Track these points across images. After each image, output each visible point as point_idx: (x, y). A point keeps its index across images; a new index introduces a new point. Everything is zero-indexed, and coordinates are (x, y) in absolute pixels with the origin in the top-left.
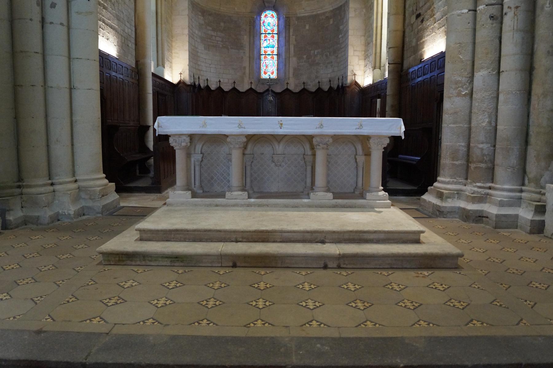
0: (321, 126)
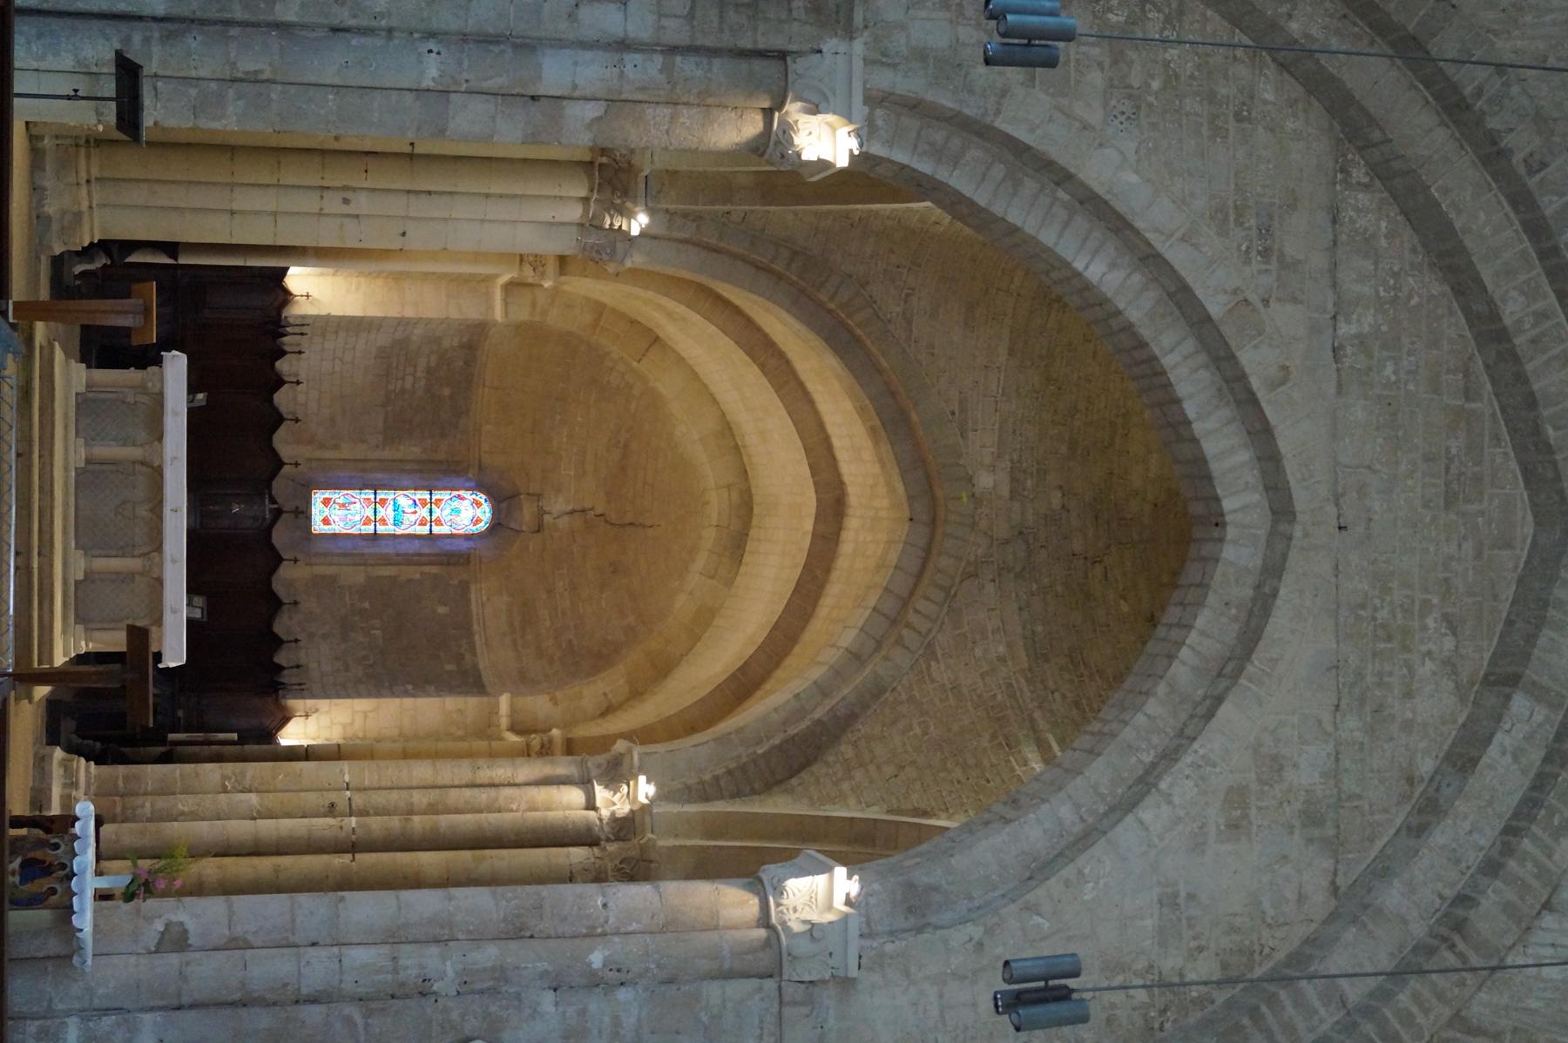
0: (174, 561)
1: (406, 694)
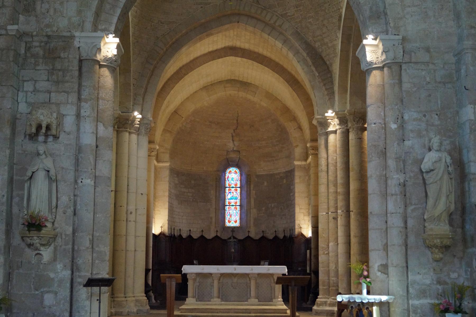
0: (252, 270)
1: (294, 195)
